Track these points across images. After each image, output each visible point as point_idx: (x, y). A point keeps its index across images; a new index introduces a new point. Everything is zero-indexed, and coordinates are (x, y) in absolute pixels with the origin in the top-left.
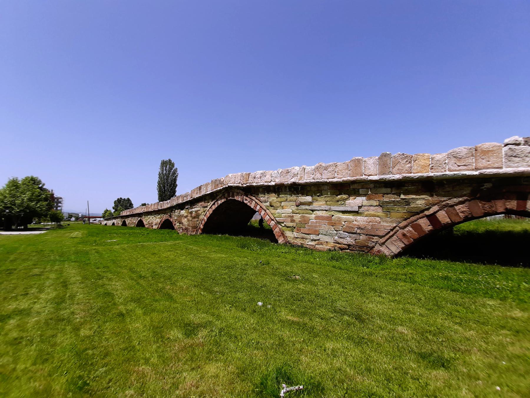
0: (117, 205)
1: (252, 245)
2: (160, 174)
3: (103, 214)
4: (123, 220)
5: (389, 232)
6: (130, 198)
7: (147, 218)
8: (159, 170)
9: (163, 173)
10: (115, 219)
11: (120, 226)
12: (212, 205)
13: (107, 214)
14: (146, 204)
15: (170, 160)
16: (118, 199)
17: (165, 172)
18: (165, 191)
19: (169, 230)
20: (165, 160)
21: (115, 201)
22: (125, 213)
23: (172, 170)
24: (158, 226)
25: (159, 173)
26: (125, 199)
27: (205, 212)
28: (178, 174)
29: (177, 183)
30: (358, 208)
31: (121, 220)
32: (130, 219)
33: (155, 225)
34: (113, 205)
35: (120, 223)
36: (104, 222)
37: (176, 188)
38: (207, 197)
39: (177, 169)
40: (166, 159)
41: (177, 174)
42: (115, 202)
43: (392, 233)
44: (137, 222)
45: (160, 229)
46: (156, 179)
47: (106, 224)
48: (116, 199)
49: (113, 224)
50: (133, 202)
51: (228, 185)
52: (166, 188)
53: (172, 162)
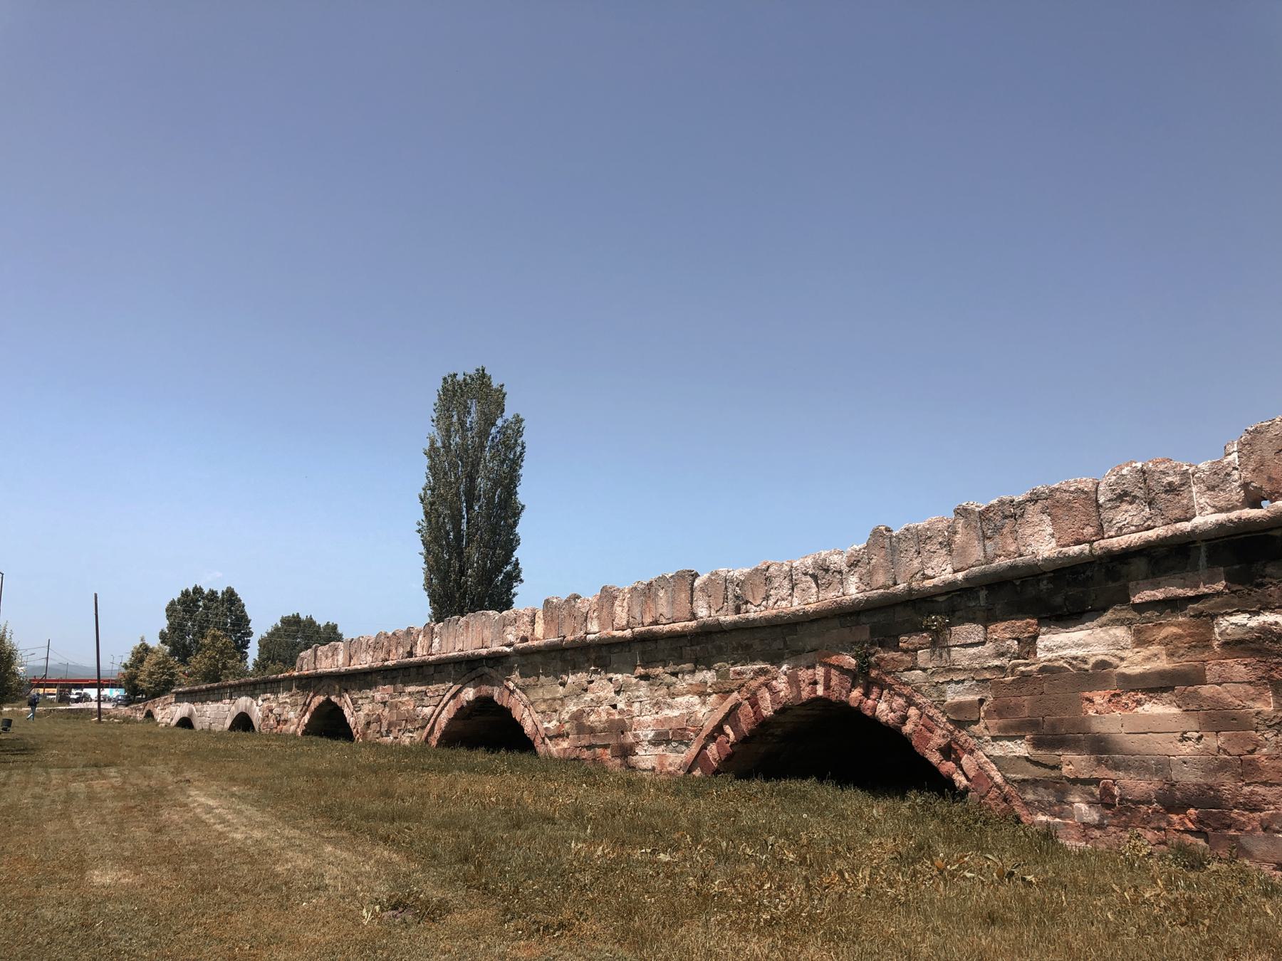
0: (180, 624)
1: (1205, 902)
2: (432, 453)
3: (126, 667)
4: (320, 699)
6: (236, 591)
7: (548, 688)
8: (433, 431)
9: (446, 446)
10: (254, 696)
11: (294, 734)
13: (147, 666)
15: (482, 376)
16: (185, 594)
18: (459, 537)
20: (460, 378)
21: (172, 603)
22: (341, 658)
24: (694, 749)
25: (433, 443)
26: (213, 593)
29: (524, 493)
31: (300, 700)
32: (378, 696)
33: (656, 742)
34: (164, 624)
35: (292, 715)
36: (173, 708)
37: (515, 524)
39: (518, 420)
40: (465, 368)
42: (171, 610)
44: (445, 717)
46: (417, 476)
47: (186, 723)
48: (177, 595)
49: (243, 722)
50: (250, 612)
52: (464, 527)
53: (495, 385)
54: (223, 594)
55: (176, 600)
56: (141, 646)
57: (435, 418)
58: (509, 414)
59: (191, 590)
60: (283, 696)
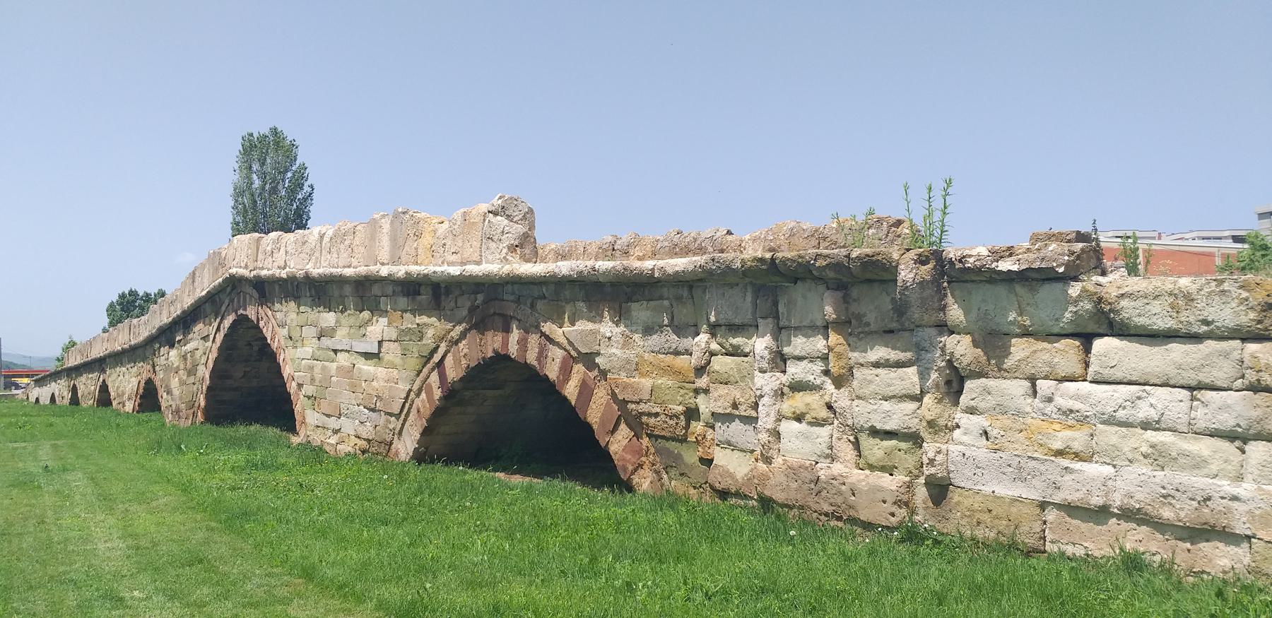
2: (239, 193)
5: (404, 403)
8: (236, 177)
12: (216, 334)
14: (1107, 240)
15: (275, 131)
16: (122, 296)
17: (257, 183)
19: (272, 432)
21: (112, 305)
23: (289, 175)
26: (147, 295)
27: (205, 354)
28: (312, 187)
30: (377, 344)
38: (207, 304)
40: (261, 128)
41: (306, 189)
43: (407, 405)
45: (138, 412)
48: (115, 298)
51: (231, 271)
54: (155, 295)
55: (114, 301)
56: (69, 343)
57: (237, 168)
58: (298, 163)
59: (127, 292)
60: (379, 328)
